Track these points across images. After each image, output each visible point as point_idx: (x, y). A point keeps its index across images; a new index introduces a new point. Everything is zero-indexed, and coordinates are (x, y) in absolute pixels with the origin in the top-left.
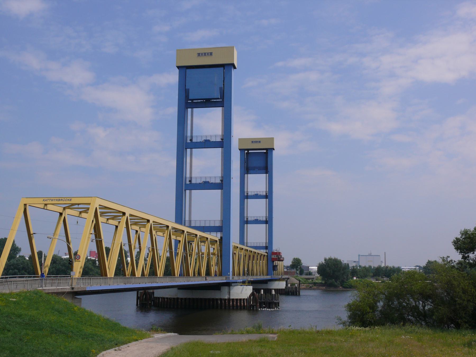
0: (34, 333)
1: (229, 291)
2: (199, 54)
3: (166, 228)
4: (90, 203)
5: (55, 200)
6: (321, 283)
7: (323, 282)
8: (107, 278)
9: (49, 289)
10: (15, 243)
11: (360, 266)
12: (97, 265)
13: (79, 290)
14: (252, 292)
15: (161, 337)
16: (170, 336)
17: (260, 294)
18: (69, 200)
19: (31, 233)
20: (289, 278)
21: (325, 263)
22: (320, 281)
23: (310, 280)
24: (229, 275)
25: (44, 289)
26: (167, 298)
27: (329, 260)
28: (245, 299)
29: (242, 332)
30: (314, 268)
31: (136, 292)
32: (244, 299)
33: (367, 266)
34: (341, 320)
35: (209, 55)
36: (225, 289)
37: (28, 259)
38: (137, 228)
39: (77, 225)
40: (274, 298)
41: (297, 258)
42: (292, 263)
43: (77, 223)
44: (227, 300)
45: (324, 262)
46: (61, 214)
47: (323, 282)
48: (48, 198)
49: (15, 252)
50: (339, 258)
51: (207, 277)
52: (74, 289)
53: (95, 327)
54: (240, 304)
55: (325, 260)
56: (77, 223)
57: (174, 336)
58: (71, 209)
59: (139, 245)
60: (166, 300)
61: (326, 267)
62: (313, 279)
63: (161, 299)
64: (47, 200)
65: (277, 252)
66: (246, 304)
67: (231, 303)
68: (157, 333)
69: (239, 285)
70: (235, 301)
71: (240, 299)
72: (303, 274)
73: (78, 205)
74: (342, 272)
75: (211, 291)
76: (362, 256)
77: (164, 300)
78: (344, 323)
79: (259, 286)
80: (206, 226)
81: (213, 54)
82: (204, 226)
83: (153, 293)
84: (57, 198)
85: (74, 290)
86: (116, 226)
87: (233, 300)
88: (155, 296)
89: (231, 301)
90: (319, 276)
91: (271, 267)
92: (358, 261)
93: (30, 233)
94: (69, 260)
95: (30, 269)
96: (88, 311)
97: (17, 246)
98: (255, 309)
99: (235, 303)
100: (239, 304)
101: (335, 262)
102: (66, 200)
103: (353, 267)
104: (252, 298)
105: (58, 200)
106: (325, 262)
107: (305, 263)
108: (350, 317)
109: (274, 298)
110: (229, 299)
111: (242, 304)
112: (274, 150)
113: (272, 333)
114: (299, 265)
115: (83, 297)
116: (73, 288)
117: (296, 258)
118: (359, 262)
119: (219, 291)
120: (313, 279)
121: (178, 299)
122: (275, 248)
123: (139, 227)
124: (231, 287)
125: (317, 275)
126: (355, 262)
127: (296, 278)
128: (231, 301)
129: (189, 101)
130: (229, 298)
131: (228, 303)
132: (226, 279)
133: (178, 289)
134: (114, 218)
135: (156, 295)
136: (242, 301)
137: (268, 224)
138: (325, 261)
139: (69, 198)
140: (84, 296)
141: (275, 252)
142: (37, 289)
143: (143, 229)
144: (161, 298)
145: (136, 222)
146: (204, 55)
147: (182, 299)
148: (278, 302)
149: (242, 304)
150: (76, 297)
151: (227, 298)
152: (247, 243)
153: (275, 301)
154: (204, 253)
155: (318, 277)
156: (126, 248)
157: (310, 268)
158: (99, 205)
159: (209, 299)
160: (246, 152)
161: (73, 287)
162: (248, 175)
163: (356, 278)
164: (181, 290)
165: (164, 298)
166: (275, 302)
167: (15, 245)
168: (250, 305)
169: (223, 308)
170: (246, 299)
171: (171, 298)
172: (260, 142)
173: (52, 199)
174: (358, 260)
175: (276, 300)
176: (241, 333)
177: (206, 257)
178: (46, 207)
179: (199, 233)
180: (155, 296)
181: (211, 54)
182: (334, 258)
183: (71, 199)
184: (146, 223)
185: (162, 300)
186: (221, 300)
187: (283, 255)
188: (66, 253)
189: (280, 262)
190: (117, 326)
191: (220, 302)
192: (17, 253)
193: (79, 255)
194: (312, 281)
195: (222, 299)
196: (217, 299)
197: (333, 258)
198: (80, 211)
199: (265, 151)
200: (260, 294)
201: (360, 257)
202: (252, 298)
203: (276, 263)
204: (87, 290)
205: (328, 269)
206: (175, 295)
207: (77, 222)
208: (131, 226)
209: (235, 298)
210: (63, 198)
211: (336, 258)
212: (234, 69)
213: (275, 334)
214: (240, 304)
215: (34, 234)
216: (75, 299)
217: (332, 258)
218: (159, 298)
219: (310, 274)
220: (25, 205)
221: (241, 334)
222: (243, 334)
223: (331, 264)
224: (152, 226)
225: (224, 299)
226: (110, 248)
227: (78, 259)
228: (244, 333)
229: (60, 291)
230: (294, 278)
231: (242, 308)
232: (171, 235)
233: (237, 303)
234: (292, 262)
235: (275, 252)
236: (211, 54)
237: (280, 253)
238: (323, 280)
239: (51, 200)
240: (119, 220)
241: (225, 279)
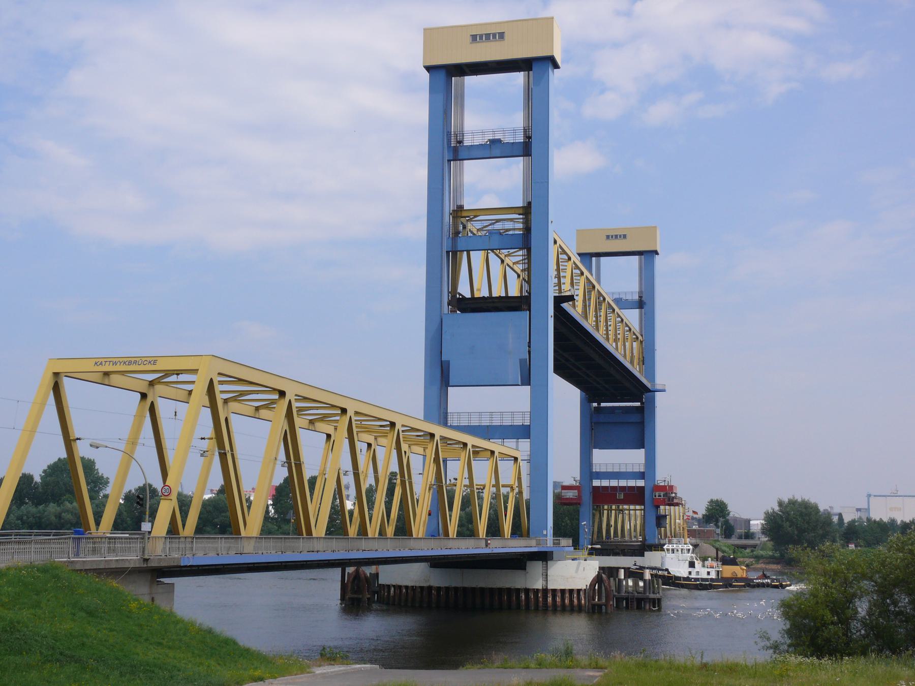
1: (545, 571)
2: (474, 38)
3: (388, 428)
4: (197, 368)
5: (120, 363)
6: (772, 557)
7: (776, 555)
8: (239, 538)
9: (84, 562)
10: (96, 468)
11: (869, 520)
12: (270, 514)
13: (163, 564)
15: (332, 672)
16: (359, 671)
17: (617, 580)
18: (152, 362)
19: (71, 438)
20: (699, 545)
21: (781, 511)
22: (771, 553)
23: (748, 550)
24: (546, 535)
25: (72, 562)
26: (407, 587)
27: (790, 504)
28: (581, 589)
29: (527, 664)
30: (757, 524)
31: (338, 571)
32: (579, 591)
33: (885, 520)
34: (768, 639)
35: (496, 38)
36: (536, 567)
37: (123, 502)
38: (370, 439)
39: (175, 419)
40: (650, 588)
41: (717, 501)
42: (706, 510)
43: (176, 415)
44: (541, 592)
45: (777, 508)
46: (144, 396)
47: (777, 555)
48: (106, 360)
49: (96, 488)
50: (813, 501)
51: (489, 540)
52: (149, 562)
53: (170, 648)
54: (571, 601)
55: (780, 504)
56: (176, 415)
58: (167, 383)
59: (374, 473)
60: (404, 591)
61: (783, 521)
62: (755, 547)
63: (392, 589)
64: (104, 363)
65: (666, 485)
66: (583, 602)
67: (550, 599)
68: (333, 663)
69: (569, 559)
70: (559, 594)
71: (571, 591)
72: (733, 536)
73: (178, 374)
74: (821, 532)
75: (482, 571)
76: (875, 496)
77: (401, 591)
78: (775, 647)
80: (493, 424)
81: (506, 36)
82: (488, 424)
83: (376, 576)
84: (125, 360)
85: (149, 565)
86: (140, 393)
87: (554, 591)
88: (380, 583)
90: (768, 540)
91: (652, 520)
92: (866, 509)
93: (69, 437)
94: (138, 497)
95: (126, 523)
96: (164, 611)
97: (100, 474)
98: (604, 610)
99: (558, 599)
100: (567, 601)
101: (804, 510)
102: (145, 363)
103: (854, 521)
104: (597, 588)
105: (127, 363)
106: (780, 509)
107: (736, 510)
108: (789, 632)
109: (650, 588)
110: (545, 591)
111: (575, 601)
112: (656, 253)
113: (594, 668)
114: (724, 517)
115: (181, 584)
116: (146, 560)
117: (715, 498)
118: (868, 510)
120: (754, 546)
122: (662, 476)
123: (408, 445)
124: (549, 562)
125: (764, 539)
126: (858, 510)
127: (714, 545)
130: (544, 588)
132: (538, 544)
133: (432, 566)
134: (323, 418)
135: (383, 580)
136: (575, 596)
138: (779, 506)
139: (151, 359)
141: (662, 484)
142: (54, 561)
143: (382, 441)
144: (394, 586)
145: (300, 409)
146: (485, 39)
147: (439, 589)
148: (660, 597)
149: (575, 601)
150: (162, 580)
151: (539, 585)
153: (652, 596)
154: (492, 486)
155: (765, 543)
156: (348, 480)
157: (752, 522)
158: (296, 395)
159: (500, 590)
161: (146, 557)
163: (856, 546)
164: (439, 569)
165: (400, 587)
166: (650, 597)
167: (96, 471)
168: (592, 605)
169: (524, 608)
170: (585, 589)
171: (416, 586)
172: (625, 236)
173: (114, 360)
174: (866, 507)
175: (654, 593)
176: (526, 666)
177: (513, 499)
178: (257, 414)
179: (471, 440)
180: (380, 583)
181: (502, 35)
182: (802, 501)
183: (155, 362)
184: (337, 418)
185: (396, 591)
186: (527, 591)
187: (680, 492)
188: (214, 490)
189: (673, 507)
190: (228, 647)
191: (525, 596)
192: (99, 488)
193: (170, 488)
194: (752, 551)
195: (529, 589)
196: (518, 591)
197: (800, 500)
198: (189, 390)
200: (617, 580)
201: (872, 499)
202: (597, 588)
204: (182, 565)
205: (786, 525)
206: (424, 579)
207: (176, 412)
208: (357, 434)
209: (568, 587)
210: (139, 359)
211: (806, 500)
212: (555, 70)
213: (602, 668)
214: (571, 601)
215: (78, 439)
216: (158, 584)
217: (797, 500)
218: (389, 586)
219: (749, 535)
220: (56, 374)
221: (525, 668)
222: (527, 668)
223: (794, 514)
224: (401, 433)
225: (534, 589)
227: (166, 494)
228: (532, 665)
229: (114, 567)
230: (710, 544)
231: (559, 609)
232: (472, 460)
233: (563, 599)
234: (707, 508)
235: (661, 484)
236: (502, 35)
237: (671, 487)
238: (775, 549)
239: (111, 363)
240: (189, 387)
241: (535, 545)
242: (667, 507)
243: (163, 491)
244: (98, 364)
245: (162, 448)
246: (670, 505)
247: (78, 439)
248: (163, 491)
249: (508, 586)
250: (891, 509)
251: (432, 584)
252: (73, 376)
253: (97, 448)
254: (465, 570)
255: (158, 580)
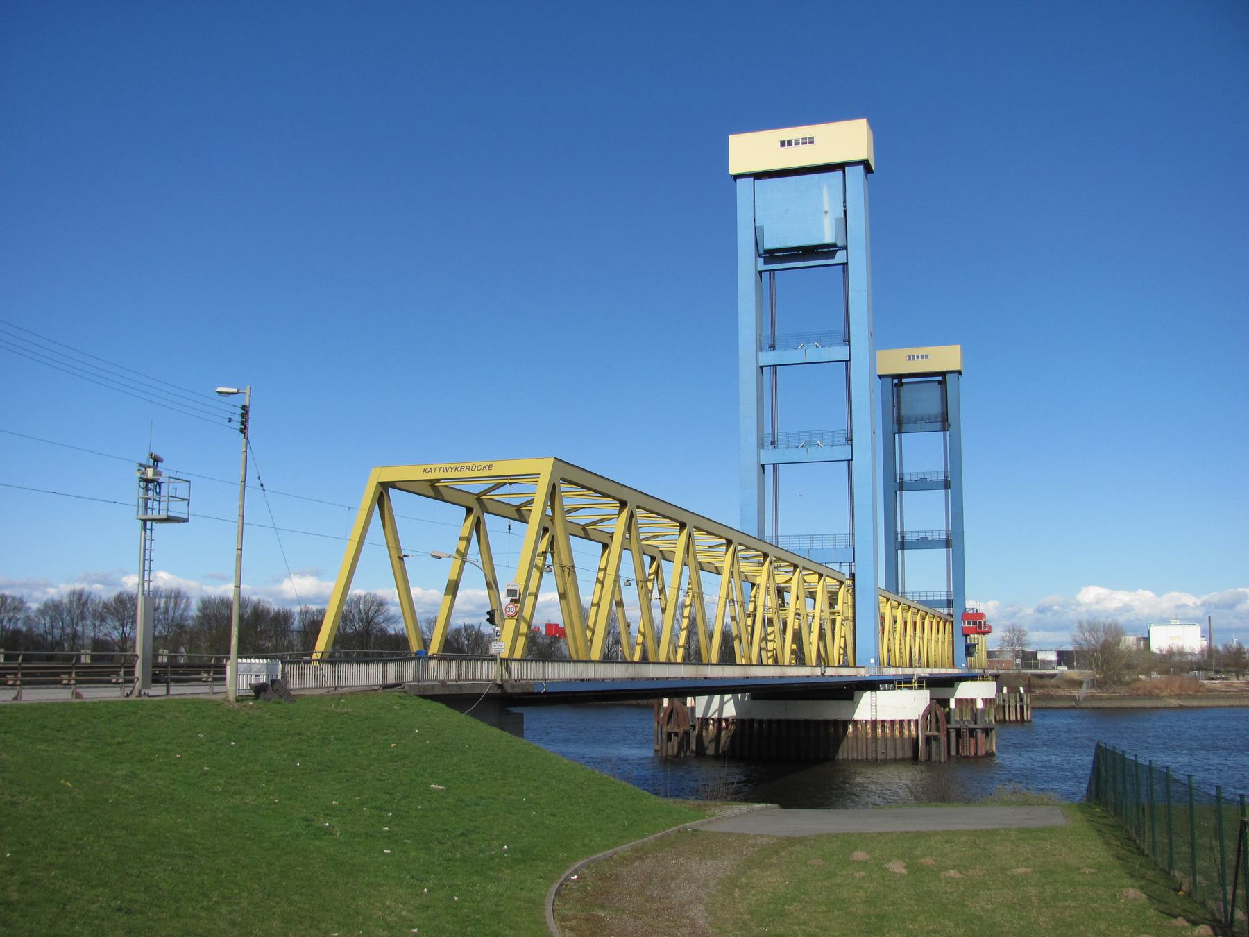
0: (886, 891)
14: (929, 703)
43: (509, 529)
56: (509, 529)
57: (762, 809)
60: (724, 724)
64: (433, 470)
79: (942, 693)
87: (883, 722)
89: (879, 727)
99: (888, 731)
100: (897, 733)
105: (459, 469)
119: (851, 702)
121: (751, 721)
128: (879, 727)
129: (389, 851)
131: (872, 731)
137: (951, 549)
140: (529, 708)
141: (971, 612)
147: (761, 722)
150: (509, 709)
152: (903, 592)
157: (1039, 657)
160: (895, 381)
162: (903, 434)
199: (940, 378)
203: (973, 638)
209: (888, 717)
226: (561, 625)
233: (893, 730)
239: (442, 470)
242: (976, 636)
243: (507, 610)
244: (427, 471)
245: (414, 623)
246: (979, 633)
247: (405, 556)
248: (507, 610)
249: (834, 717)
250: (1171, 638)
251: (753, 717)
252: (403, 487)
253: (440, 558)
254: (790, 702)
255: (507, 709)
